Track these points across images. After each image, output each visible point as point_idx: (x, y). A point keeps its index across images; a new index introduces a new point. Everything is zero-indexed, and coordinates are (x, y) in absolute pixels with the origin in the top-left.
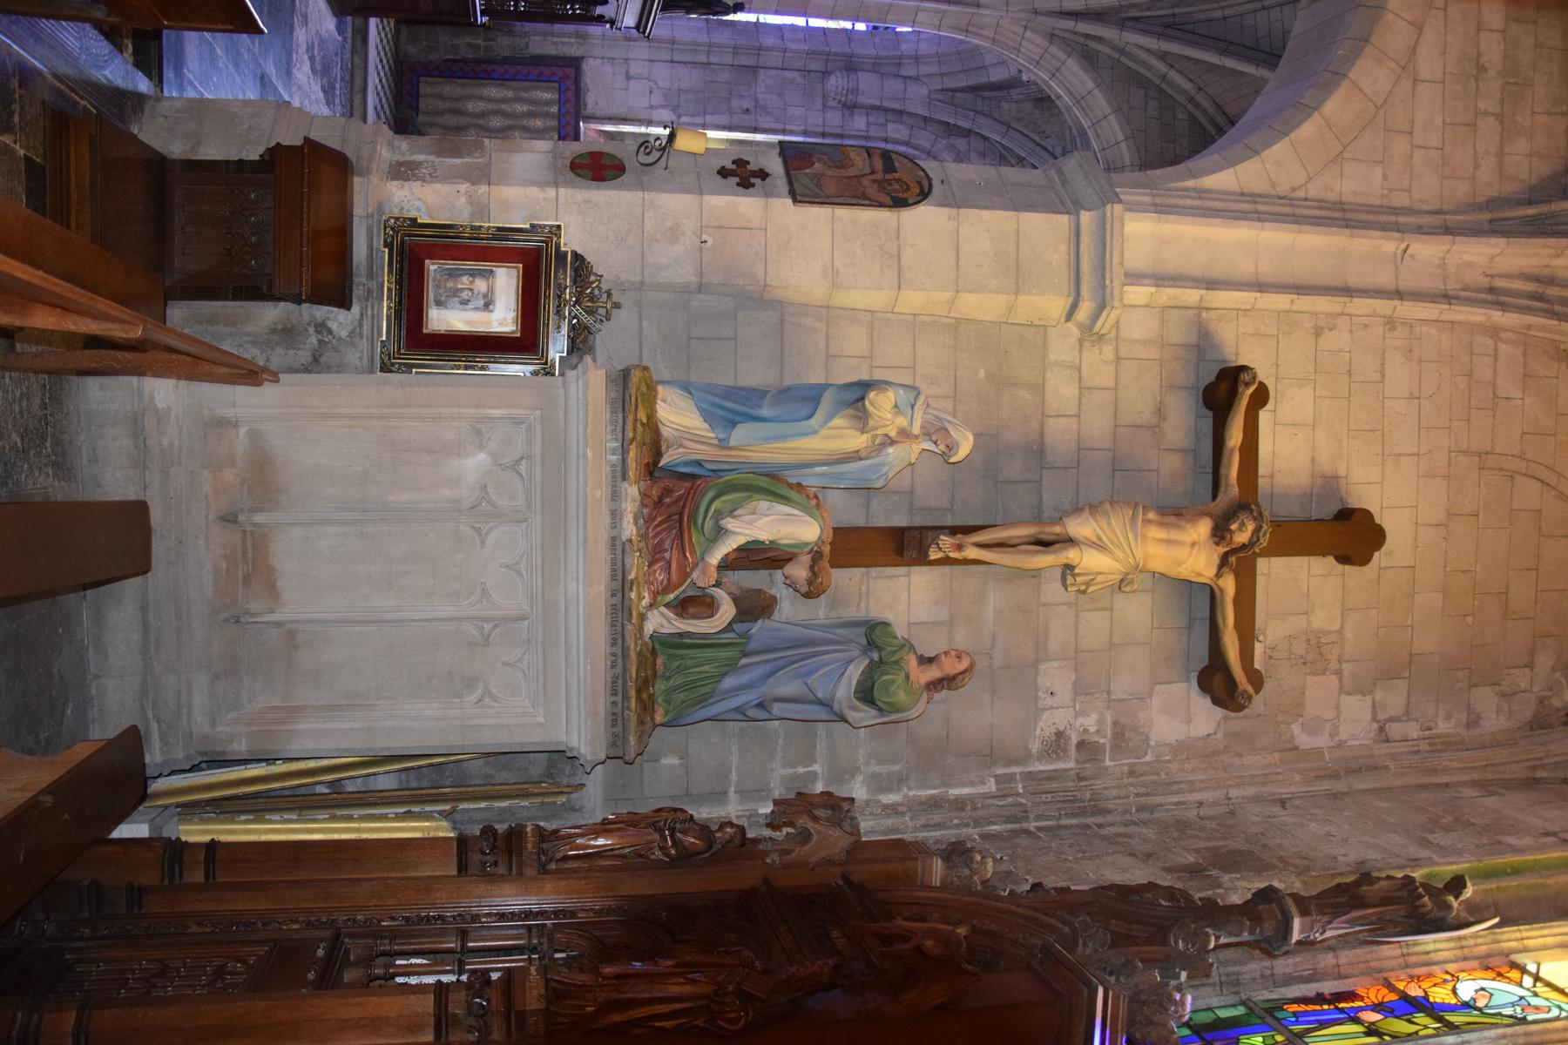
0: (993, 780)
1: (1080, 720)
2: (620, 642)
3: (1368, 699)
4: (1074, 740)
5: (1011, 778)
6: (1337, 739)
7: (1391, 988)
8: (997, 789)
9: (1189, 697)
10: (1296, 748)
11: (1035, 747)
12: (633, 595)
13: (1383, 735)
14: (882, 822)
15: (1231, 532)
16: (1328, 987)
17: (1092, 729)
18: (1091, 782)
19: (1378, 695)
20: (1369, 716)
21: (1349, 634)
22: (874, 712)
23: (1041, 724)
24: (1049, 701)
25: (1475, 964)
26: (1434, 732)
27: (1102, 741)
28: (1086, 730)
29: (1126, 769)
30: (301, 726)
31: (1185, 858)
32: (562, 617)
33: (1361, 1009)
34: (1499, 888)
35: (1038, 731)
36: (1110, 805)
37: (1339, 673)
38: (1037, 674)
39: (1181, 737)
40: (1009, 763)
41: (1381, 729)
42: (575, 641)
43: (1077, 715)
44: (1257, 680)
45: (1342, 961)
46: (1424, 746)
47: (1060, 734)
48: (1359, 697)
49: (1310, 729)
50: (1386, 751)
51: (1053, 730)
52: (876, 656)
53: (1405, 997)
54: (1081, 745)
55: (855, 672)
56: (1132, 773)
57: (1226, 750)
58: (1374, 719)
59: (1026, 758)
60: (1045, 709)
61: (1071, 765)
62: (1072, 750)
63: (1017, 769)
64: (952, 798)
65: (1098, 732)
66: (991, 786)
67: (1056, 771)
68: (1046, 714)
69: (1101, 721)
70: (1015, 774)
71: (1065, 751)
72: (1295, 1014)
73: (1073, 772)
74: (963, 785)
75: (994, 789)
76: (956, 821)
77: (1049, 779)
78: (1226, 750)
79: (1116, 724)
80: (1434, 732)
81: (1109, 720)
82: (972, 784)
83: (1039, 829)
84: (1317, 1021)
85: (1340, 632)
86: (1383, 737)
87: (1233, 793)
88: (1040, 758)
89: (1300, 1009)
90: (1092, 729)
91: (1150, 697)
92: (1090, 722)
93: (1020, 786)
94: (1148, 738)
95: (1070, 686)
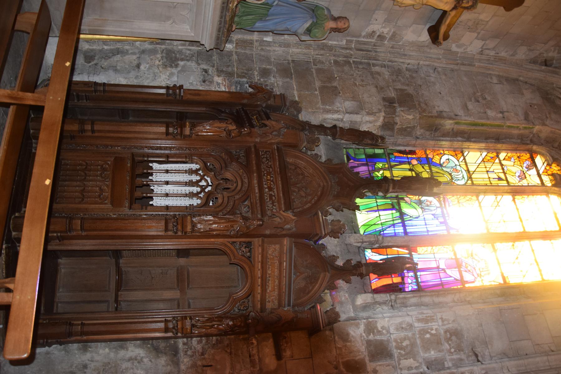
0: (345, 41)
1: (382, 29)
2: (224, 18)
3: (484, 42)
4: (378, 34)
5: (351, 41)
6: (465, 50)
7: (425, 153)
8: (346, 44)
9: (423, 30)
10: (451, 50)
11: (364, 34)
12: (230, 5)
13: (481, 53)
14: (304, 50)
15: (463, 2)
16: (408, 149)
17: (385, 33)
18: (377, 47)
19: (487, 42)
20: (481, 46)
21: (490, 23)
22: (309, 37)
23: (369, 28)
24: (375, 22)
25: (452, 149)
26: (499, 55)
27: (387, 36)
28: (383, 32)
29: (391, 46)
30: (107, 28)
31: (391, 93)
32: (204, 7)
33: (412, 158)
34: (474, 129)
35: (367, 30)
36: (380, 59)
37: (479, 33)
38: (374, 13)
39: (414, 40)
40: (353, 36)
41: (482, 51)
42: (207, 16)
43: (382, 27)
44: (446, 37)
45: (417, 143)
46: (492, 59)
47: (374, 32)
48: (481, 41)
49: (458, 46)
50: (479, 57)
51: (372, 30)
52: (315, 21)
53: (427, 158)
54: (379, 36)
55: (307, 25)
56: (392, 47)
57: (427, 46)
58: (482, 48)
59: (360, 36)
60: (372, 24)
61: (373, 41)
62: (376, 37)
63: (355, 39)
64: (330, 45)
65: (387, 34)
66: (344, 42)
67: (368, 42)
68: (372, 25)
69: (390, 31)
70: (353, 40)
71: (373, 36)
72: (396, 157)
73: (373, 43)
74: (334, 41)
75: (344, 44)
76: (328, 55)
77: (364, 44)
78: (427, 46)
79: (394, 32)
80: (499, 55)
81: (392, 31)
82: (338, 41)
83: (354, 62)
84: (400, 161)
85: (488, 22)
86: (481, 53)
87: (421, 62)
88: (364, 37)
89: (398, 155)
90: (385, 33)
91: (410, 27)
92: (386, 31)
93: (353, 44)
94: (403, 38)
95: (384, 19)
